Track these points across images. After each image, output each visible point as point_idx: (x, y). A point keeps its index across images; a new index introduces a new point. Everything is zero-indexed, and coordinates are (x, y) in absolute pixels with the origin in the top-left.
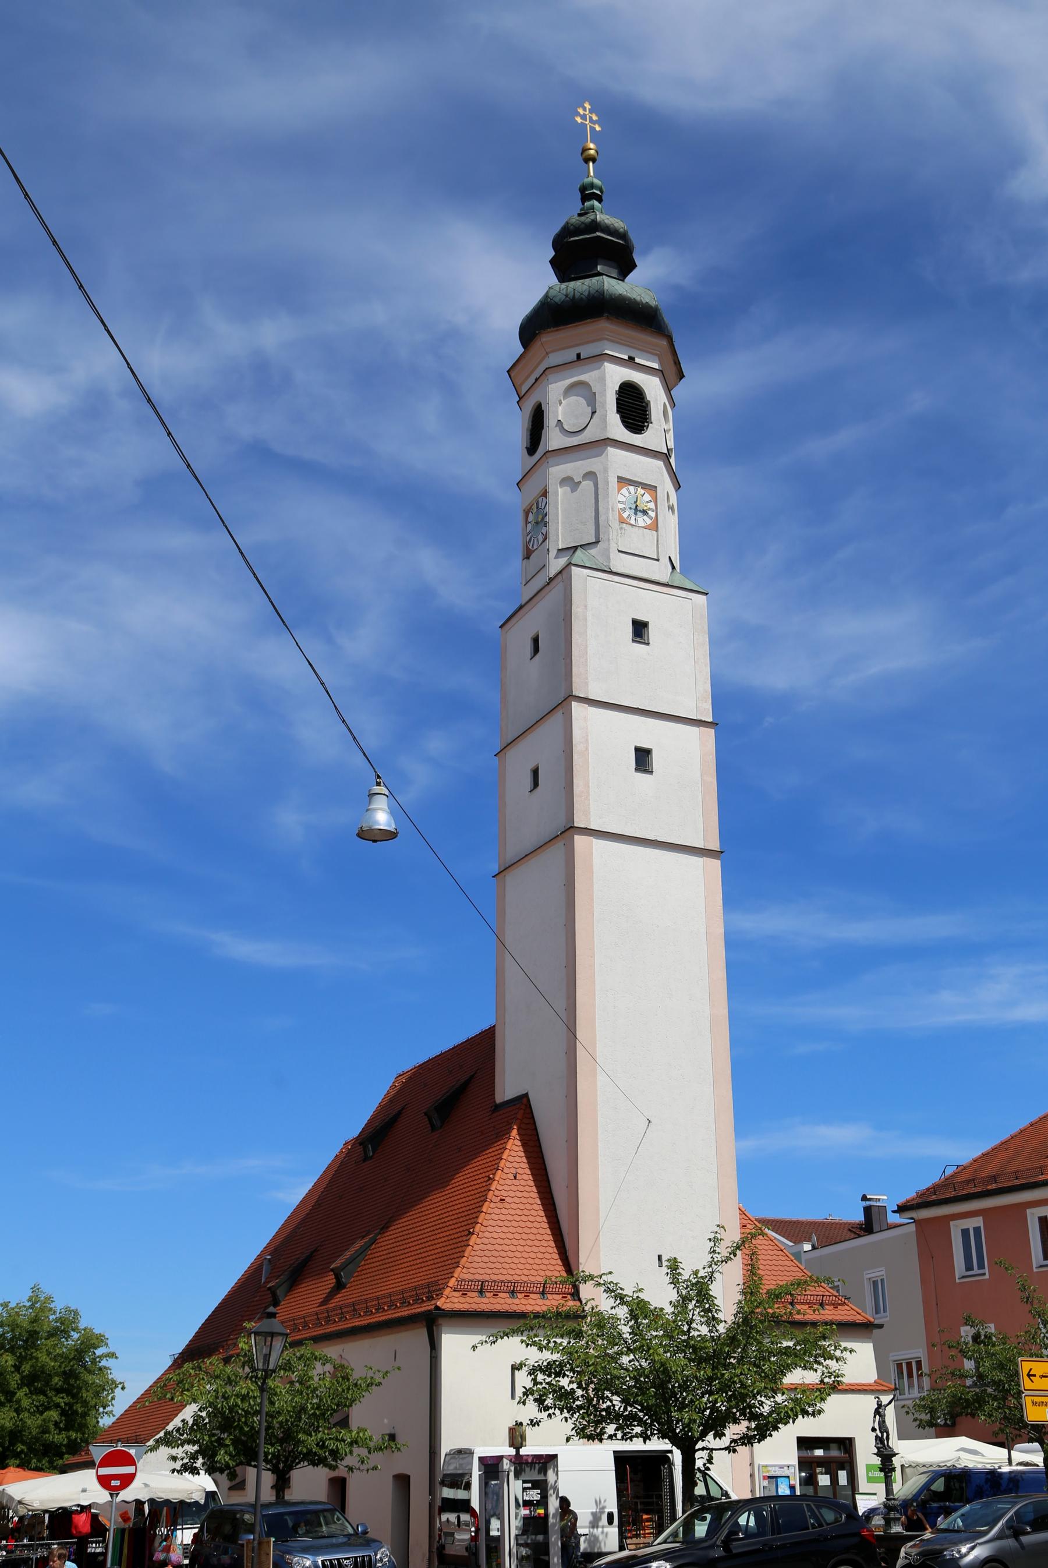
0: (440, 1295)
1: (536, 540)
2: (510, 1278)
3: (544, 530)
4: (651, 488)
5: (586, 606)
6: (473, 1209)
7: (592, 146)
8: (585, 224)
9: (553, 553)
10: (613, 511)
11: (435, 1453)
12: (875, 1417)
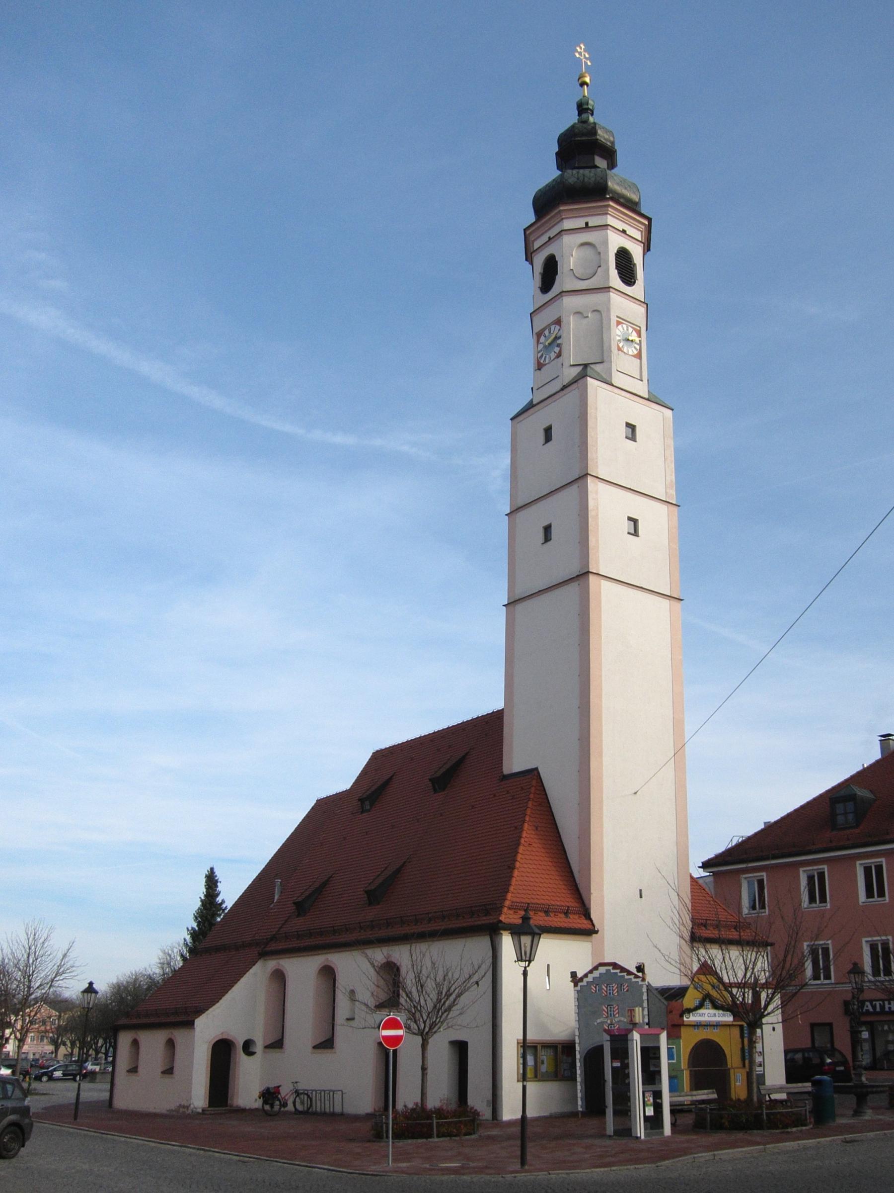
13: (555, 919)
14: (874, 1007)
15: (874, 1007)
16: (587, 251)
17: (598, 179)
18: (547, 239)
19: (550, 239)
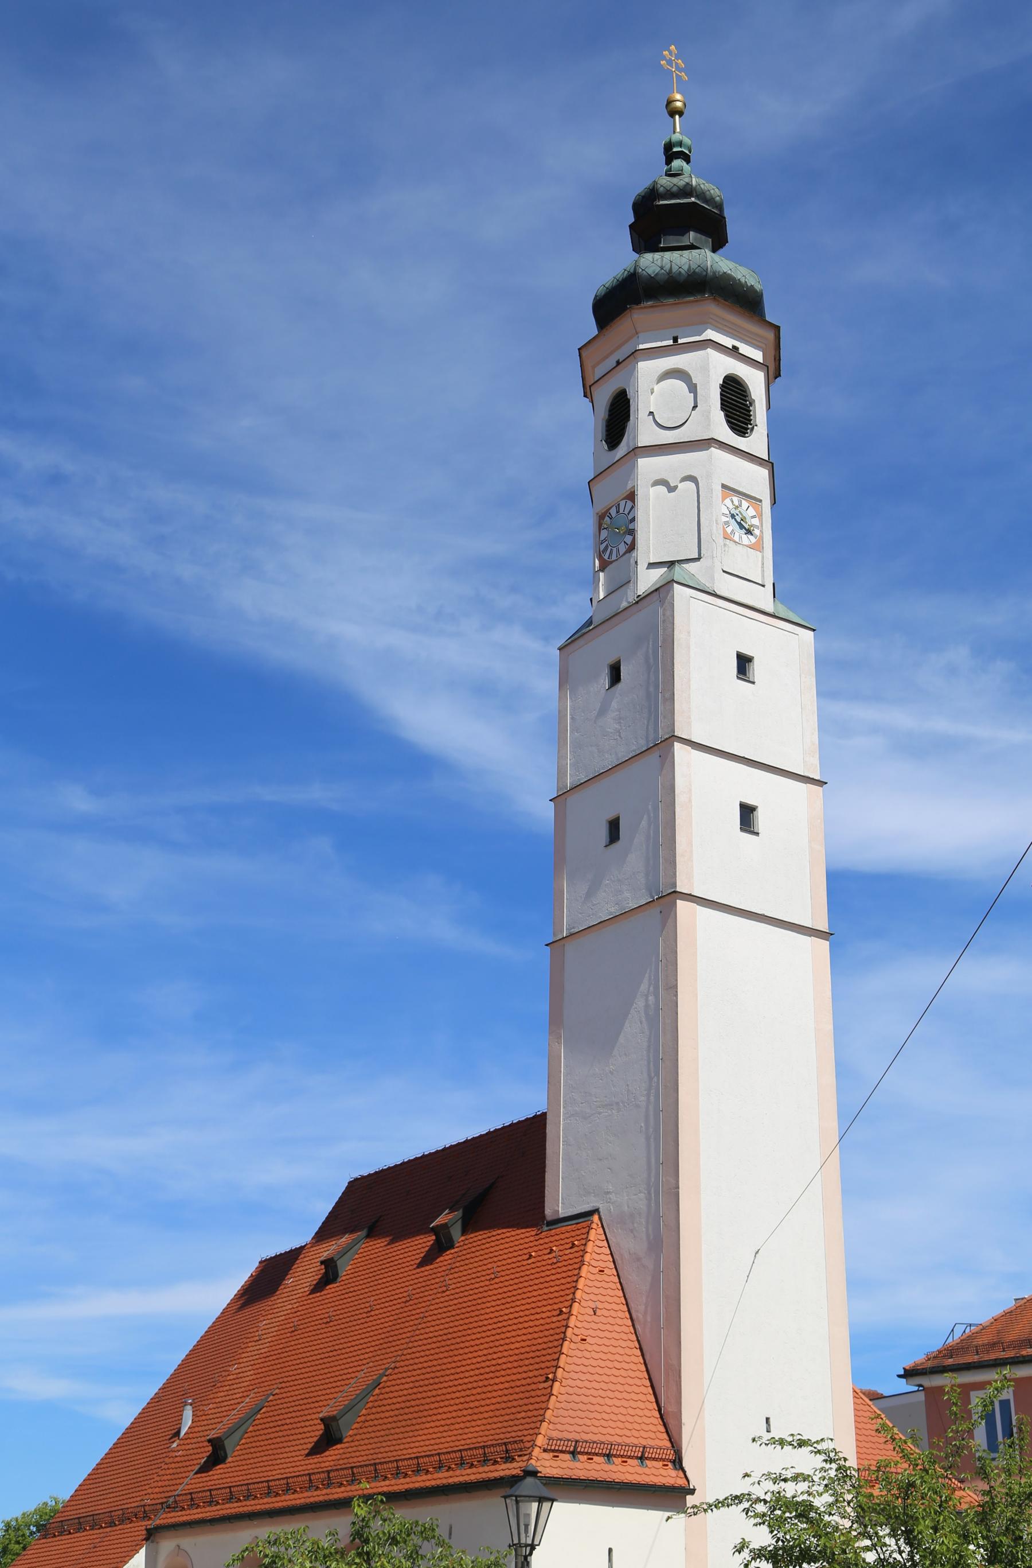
1: (615, 550)
2: (603, 1439)
5: (689, 633)
6: (276, 1340)
7: (678, 97)
9: (642, 566)
10: (717, 524)
13: (620, 1468)
16: (678, 386)
17: (694, 266)
19: (618, 363)
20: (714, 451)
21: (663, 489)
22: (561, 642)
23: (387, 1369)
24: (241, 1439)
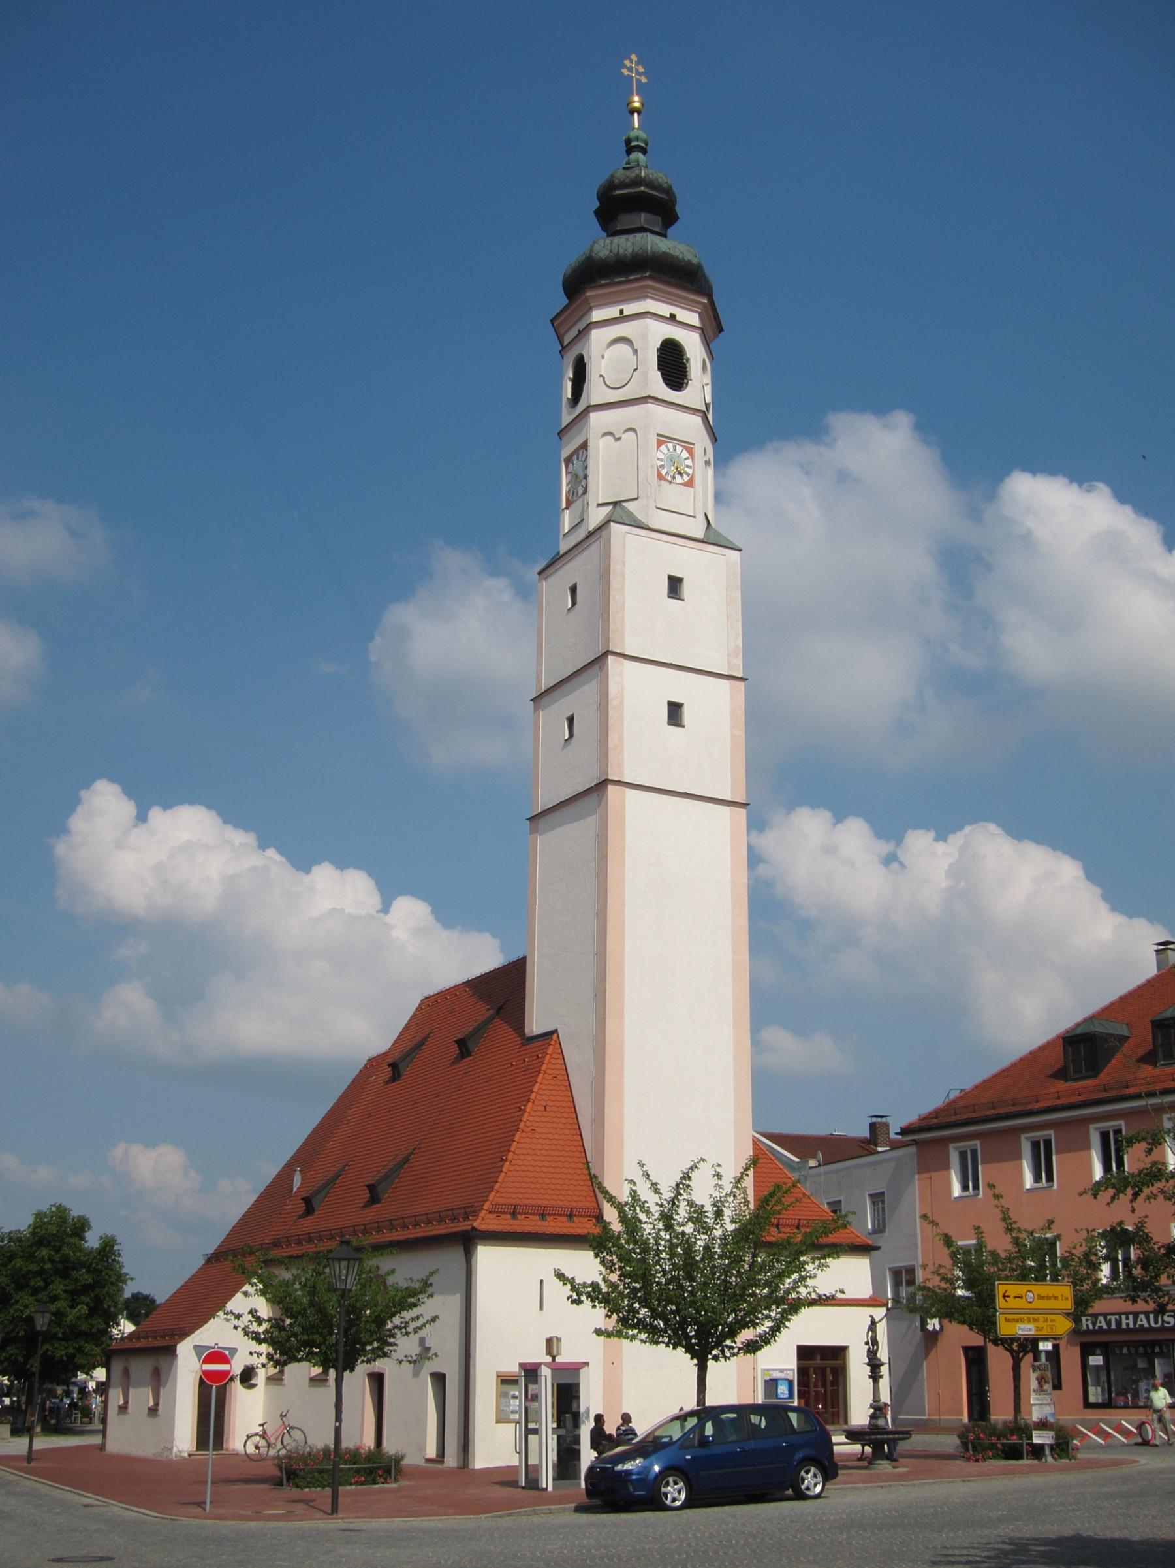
0: (475, 1214)
2: (540, 1202)
3: (583, 483)
4: (689, 447)
8: (630, 179)
9: (592, 507)
11: (469, 1355)
12: (868, 1332)
14: (1109, 1323)
15: (1109, 1323)
16: (623, 348)
17: (637, 249)
18: (577, 333)
20: (651, 407)
21: (609, 438)
22: (539, 568)
23: (414, 1149)
24: (325, 1198)
